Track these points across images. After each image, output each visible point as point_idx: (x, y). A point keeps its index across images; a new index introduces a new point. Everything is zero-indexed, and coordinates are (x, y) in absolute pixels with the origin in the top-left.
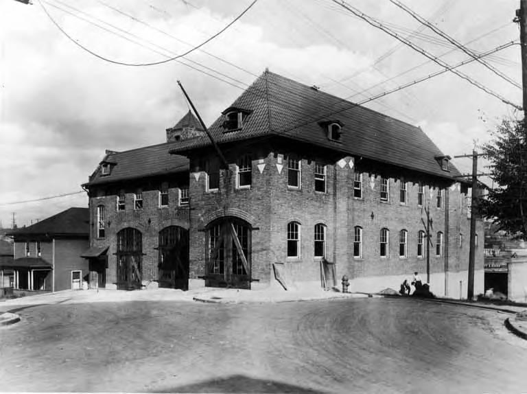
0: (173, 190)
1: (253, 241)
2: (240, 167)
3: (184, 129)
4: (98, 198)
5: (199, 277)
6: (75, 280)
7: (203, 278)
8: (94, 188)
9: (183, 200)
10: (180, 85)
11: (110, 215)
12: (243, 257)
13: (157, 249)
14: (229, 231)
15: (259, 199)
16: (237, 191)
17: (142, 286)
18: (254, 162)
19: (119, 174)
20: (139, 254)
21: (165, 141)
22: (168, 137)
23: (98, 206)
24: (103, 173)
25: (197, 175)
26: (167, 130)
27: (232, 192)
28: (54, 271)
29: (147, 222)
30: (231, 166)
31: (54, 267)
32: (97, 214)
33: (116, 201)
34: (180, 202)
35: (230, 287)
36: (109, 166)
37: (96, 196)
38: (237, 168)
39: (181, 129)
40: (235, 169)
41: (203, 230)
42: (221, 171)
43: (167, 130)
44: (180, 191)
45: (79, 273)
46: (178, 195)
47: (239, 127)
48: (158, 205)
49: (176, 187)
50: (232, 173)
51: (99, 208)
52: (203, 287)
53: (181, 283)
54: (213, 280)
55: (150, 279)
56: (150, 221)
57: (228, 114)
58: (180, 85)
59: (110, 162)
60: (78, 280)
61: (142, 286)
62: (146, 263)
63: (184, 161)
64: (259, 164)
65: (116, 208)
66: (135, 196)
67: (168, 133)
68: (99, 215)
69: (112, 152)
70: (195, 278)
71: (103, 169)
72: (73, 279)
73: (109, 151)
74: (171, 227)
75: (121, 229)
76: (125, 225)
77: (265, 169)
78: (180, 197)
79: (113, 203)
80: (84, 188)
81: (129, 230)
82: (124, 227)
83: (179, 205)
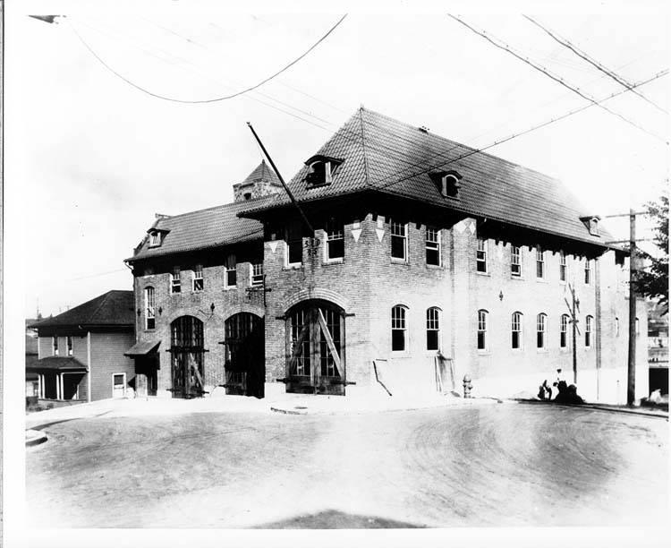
3: (256, 184)
6: (116, 386)
9: (255, 278)
10: (251, 127)
12: (334, 353)
13: (223, 343)
14: (315, 319)
19: (171, 245)
20: (200, 351)
26: (234, 186)
28: (89, 375)
29: (209, 308)
30: (317, 233)
31: (89, 370)
32: (144, 298)
35: (318, 393)
36: (159, 234)
38: (326, 234)
39: (252, 185)
42: (305, 239)
43: (234, 186)
44: (251, 266)
45: (122, 376)
47: (327, 181)
50: (318, 242)
51: (146, 291)
54: (295, 383)
56: (213, 307)
60: (122, 386)
64: (353, 229)
65: (169, 290)
70: (273, 381)
74: (239, 314)
75: (176, 317)
76: (181, 313)
78: (252, 274)
80: (128, 263)
81: (187, 318)
82: (179, 315)
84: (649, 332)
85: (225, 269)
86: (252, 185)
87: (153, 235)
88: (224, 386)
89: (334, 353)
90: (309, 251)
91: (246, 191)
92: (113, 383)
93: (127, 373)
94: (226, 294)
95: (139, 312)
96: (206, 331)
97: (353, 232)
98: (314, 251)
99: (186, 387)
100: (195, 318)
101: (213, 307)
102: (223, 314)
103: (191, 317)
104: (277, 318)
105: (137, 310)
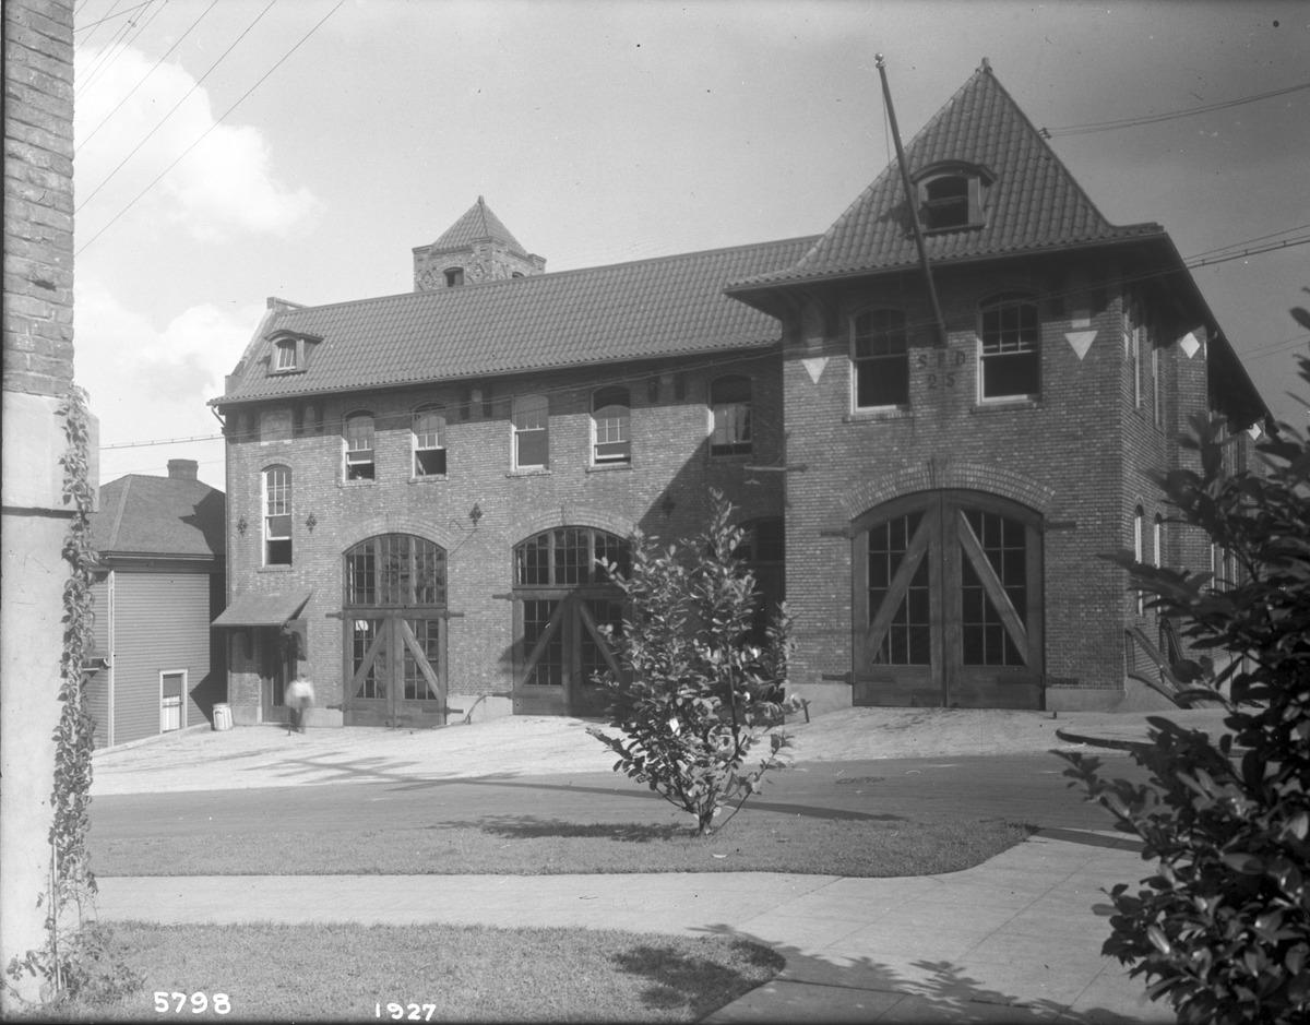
0: (569, 419)
1: (1050, 562)
2: (986, 342)
3: (477, 249)
4: (264, 444)
5: (827, 678)
6: (168, 700)
7: (846, 679)
8: (242, 418)
9: (601, 449)
10: (882, 70)
11: (332, 499)
13: (508, 597)
15: (1076, 438)
16: (975, 412)
17: (447, 711)
18: (1048, 329)
19: (326, 374)
21: (412, 291)
22: (418, 271)
23: (264, 470)
24: (278, 368)
25: (815, 367)
26: (416, 251)
27: (964, 414)
28: (112, 673)
29: (465, 516)
30: (954, 340)
31: (111, 662)
32: (258, 491)
33: (338, 454)
34: (594, 455)
36: (301, 344)
37: (259, 440)
39: (467, 250)
40: (973, 348)
41: (843, 533)
42: (914, 355)
43: (416, 251)
44: (593, 423)
45: (180, 676)
46: (587, 435)
47: (972, 220)
48: (509, 464)
49: (580, 411)
51: (264, 475)
52: (845, 707)
53: (424, 705)
55: (480, 691)
56: (475, 514)
57: (930, 179)
58: (882, 70)
59: (290, 333)
61: (447, 711)
62: (460, 642)
63: (763, 329)
64: (1071, 330)
65: (338, 474)
66: (414, 439)
67: (418, 260)
68: (265, 497)
69: (285, 304)
71: (278, 354)
72: (165, 697)
73: (279, 302)
74: (558, 532)
75: (360, 538)
77: (1094, 345)
78: (594, 439)
79: (328, 460)
80: (216, 410)
82: (370, 533)
83: (592, 464)
84: (553, 683)
85: (514, 429)
86: (467, 250)
87: (280, 345)
88: (508, 695)
89: (428, 671)
90: (931, 378)
91: (449, 263)
92: (161, 694)
93: (189, 668)
94: (516, 483)
95: (242, 527)
96: (455, 571)
97: (1070, 337)
98: (948, 378)
99: (888, 662)
100: (421, 540)
101: (475, 514)
102: (510, 527)
103: (407, 537)
104: (824, 534)
105: (234, 521)
